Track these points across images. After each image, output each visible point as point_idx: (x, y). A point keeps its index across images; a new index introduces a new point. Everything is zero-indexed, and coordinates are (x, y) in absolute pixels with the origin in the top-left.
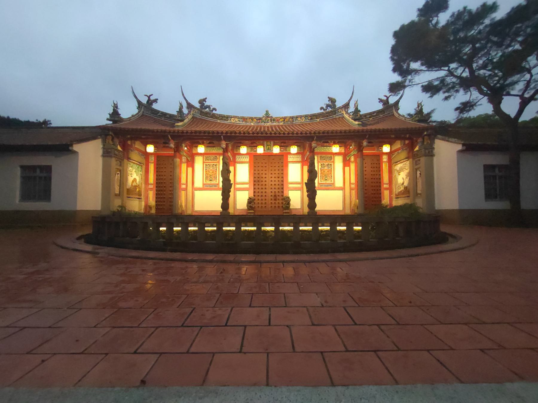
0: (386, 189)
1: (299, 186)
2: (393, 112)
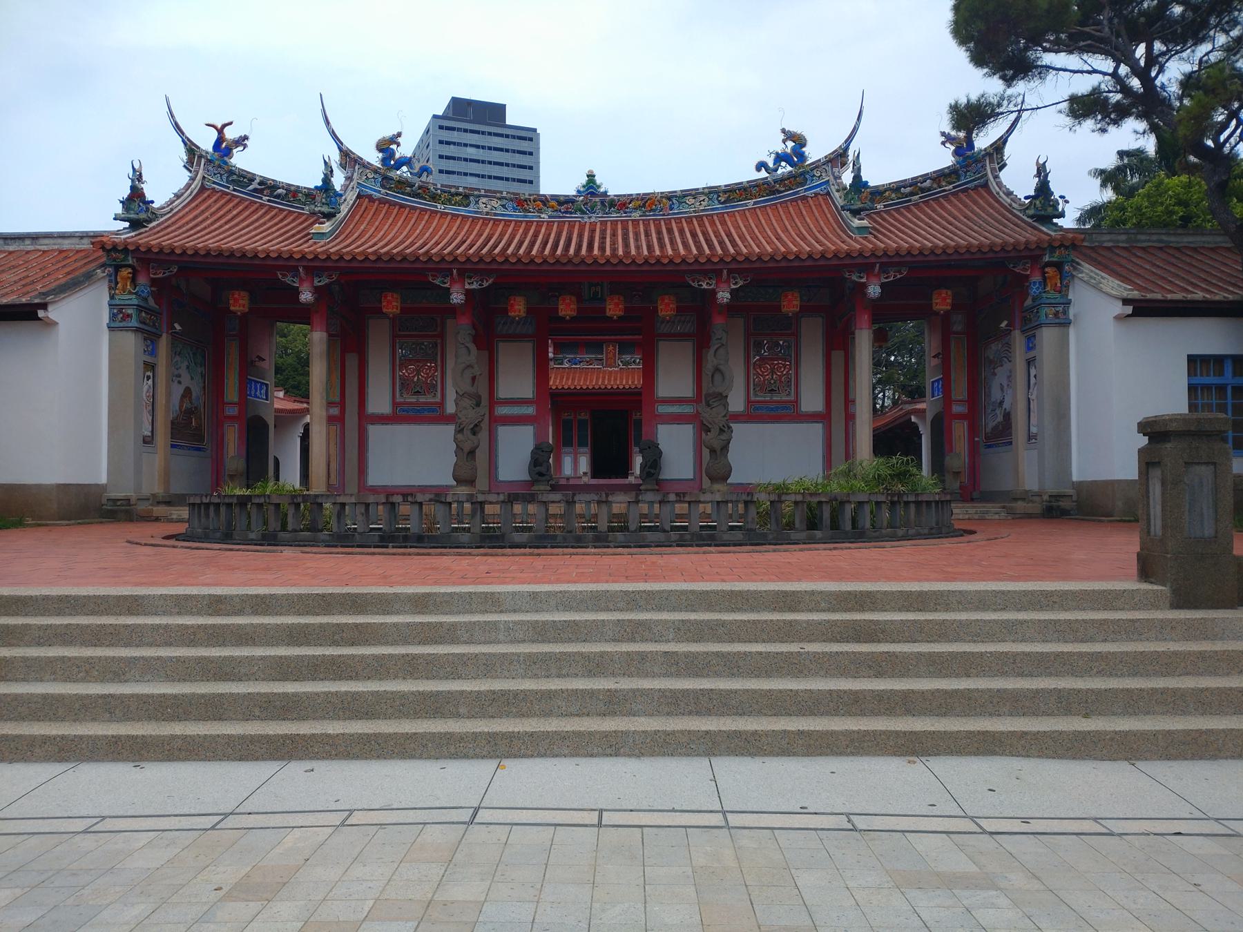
0: (960, 417)
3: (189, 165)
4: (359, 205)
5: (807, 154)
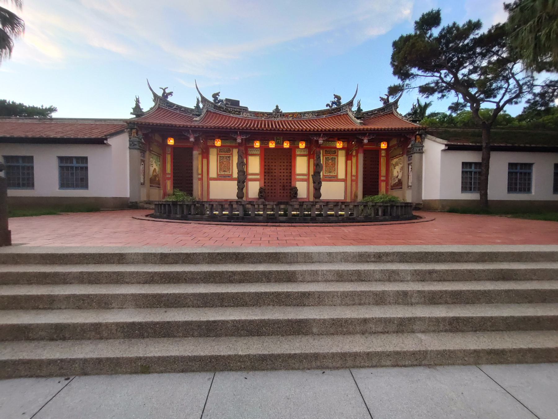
0: (383, 181)
1: (306, 177)
2: (392, 110)
3: (154, 101)
4: (207, 114)
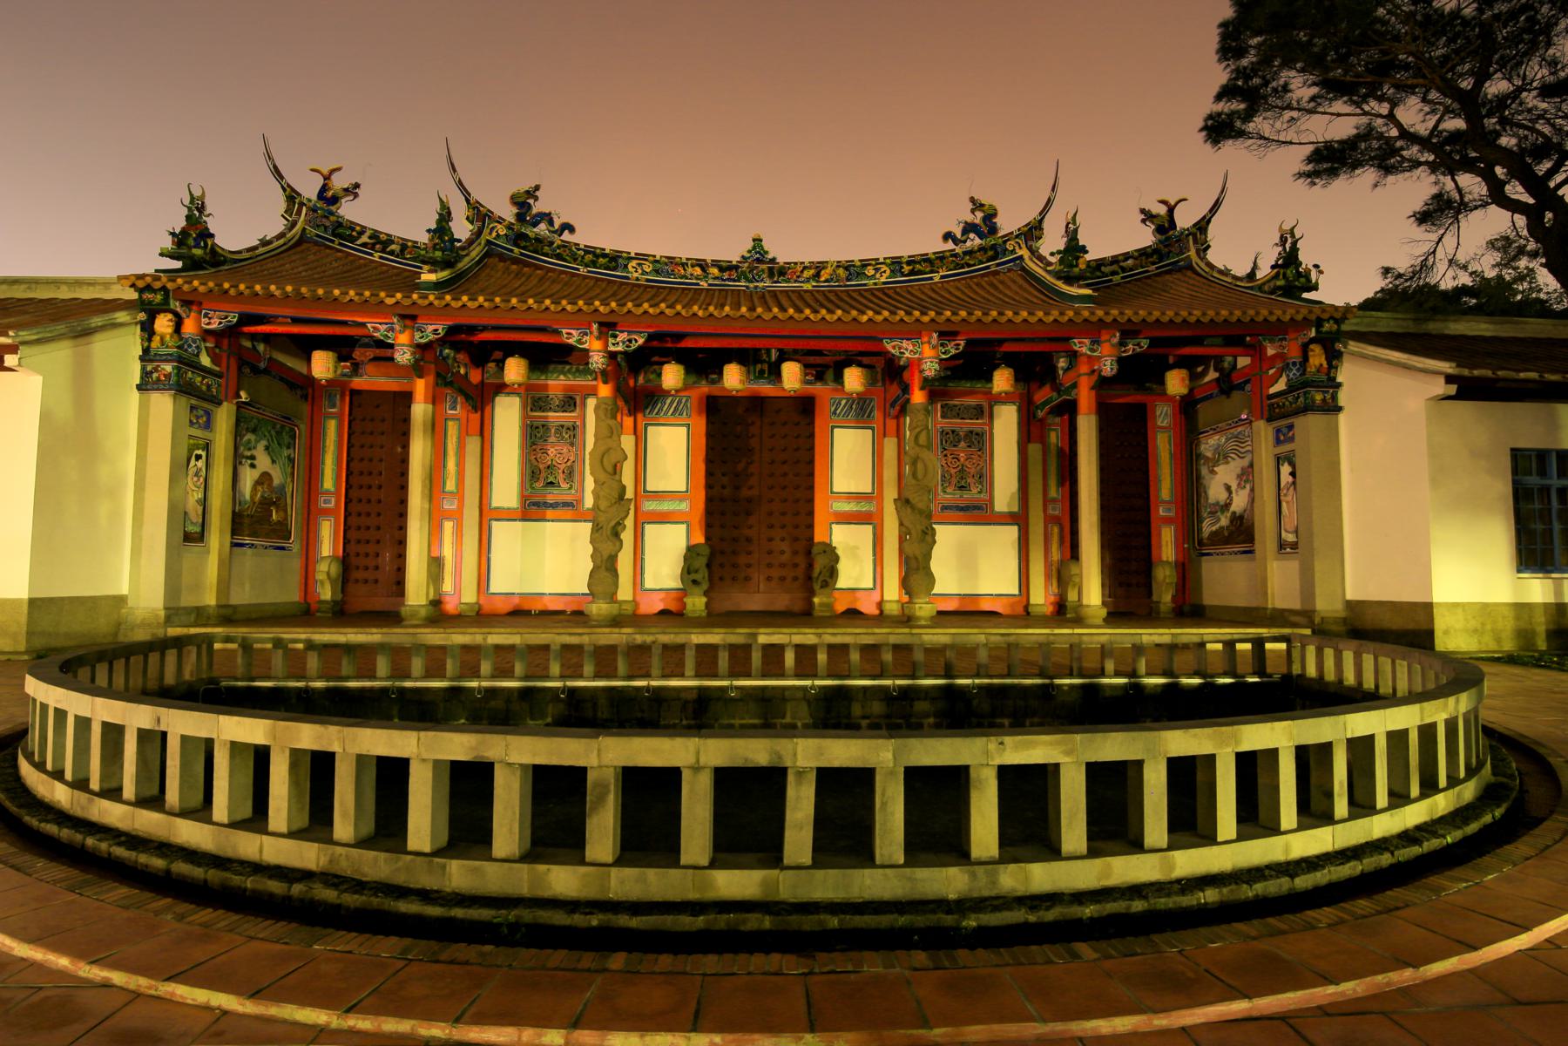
5: (998, 224)
